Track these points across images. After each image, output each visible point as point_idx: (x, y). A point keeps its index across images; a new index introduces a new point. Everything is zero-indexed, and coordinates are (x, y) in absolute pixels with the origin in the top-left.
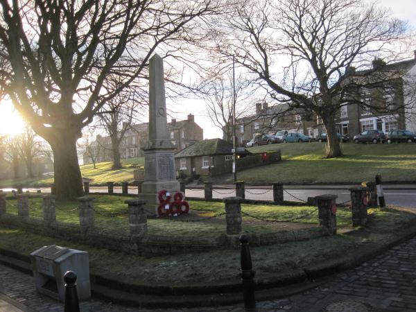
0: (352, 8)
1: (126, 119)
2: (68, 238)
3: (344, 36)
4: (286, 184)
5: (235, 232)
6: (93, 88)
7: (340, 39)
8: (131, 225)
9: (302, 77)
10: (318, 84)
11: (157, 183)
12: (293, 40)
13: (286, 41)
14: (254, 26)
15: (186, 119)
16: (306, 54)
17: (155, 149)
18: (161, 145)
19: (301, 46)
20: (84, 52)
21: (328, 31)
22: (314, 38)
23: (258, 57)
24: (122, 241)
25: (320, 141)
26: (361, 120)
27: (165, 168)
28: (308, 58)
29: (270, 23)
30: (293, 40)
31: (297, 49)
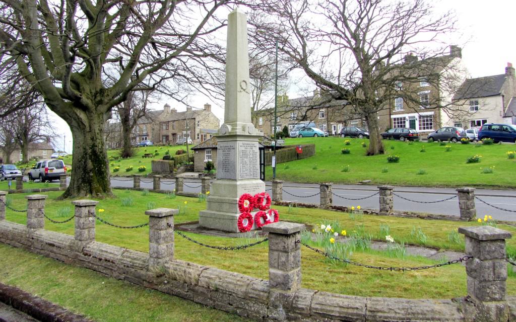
0: (195, 63)
1: (140, 106)
2: (123, 276)
3: (388, 27)
4: (336, 183)
5: (497, 296)
6: (125, 64)
7: (384, 28)
8: (273, 271)
9: (341, 66)
10: (359, 74)
11: (238, 183)
12: (336, 26)
13: (330, 28)
14: (293, 11)
15: (503, 72)
16: (349, 42)
17: (236, 136)
18: (244, 130)
19: (344, 33)
20: (115, 16)
21: (371, 19)
22: (358, 26)
23: (295, 42)
24: (246, 297)
25: (343, 136)
26: (393, 117)
27: (248, 162)
28: (351, 48)
29: (312, 8)
30: (336, 26)
31: (341, 36)
